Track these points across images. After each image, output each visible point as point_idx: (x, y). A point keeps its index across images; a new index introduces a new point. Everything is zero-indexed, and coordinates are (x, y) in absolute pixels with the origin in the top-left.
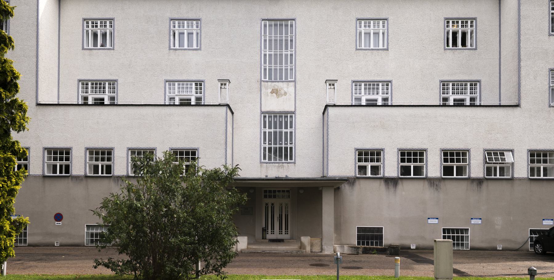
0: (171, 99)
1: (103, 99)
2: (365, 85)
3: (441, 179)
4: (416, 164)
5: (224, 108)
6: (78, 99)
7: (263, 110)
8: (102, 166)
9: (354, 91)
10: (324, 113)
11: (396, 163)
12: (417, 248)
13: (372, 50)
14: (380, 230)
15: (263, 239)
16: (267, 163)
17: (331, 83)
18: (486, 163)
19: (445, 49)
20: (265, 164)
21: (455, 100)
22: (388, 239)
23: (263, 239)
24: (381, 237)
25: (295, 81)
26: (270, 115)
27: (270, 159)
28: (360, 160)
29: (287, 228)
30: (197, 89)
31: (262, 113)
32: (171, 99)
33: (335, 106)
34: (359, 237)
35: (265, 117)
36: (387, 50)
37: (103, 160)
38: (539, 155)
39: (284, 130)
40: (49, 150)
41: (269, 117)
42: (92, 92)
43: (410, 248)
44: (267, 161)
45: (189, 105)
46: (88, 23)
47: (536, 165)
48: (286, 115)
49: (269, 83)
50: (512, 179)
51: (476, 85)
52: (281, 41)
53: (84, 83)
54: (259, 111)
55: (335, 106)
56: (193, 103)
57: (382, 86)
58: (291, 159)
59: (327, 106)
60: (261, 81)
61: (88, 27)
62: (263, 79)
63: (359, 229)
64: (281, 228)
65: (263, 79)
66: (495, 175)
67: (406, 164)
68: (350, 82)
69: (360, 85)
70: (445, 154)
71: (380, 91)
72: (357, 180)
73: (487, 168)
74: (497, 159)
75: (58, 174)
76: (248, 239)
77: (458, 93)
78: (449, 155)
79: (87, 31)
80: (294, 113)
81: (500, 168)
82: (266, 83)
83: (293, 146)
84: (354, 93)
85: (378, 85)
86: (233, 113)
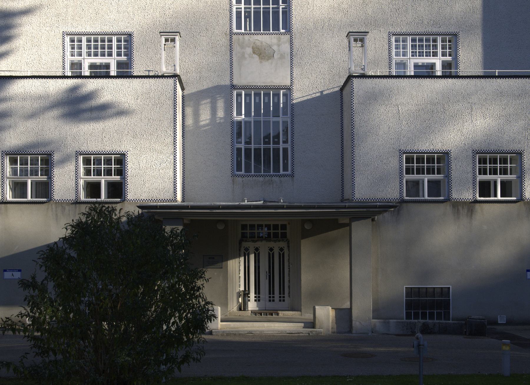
0: (73, 65)
1: (107, 66)
2: (413, 40)
4: (432, 177)
5: (171, 81)
6: (64, 68)
9: (394, 51)
12: (509, 322)
16: (242, 176)
17: (358, 37)
20: (240, 179)
21: (416, 66)
26: (248, 91)
27: (248, 169)
28: (483, 171)
29: (282, 291)
30: (73, 48)
32: (73, 65)
33: (363, 76)
39: (272, 119)
40: (123, 155)
42: (414, 54)
43: (496, 323)
44: (243, 172)
45: (107, 76)
48: (276, 92)
49: (247, 37)
53: (75, 38)
55: (363, 76)
56: (113, 73)
57: (396, 41)
58: (285, 169)
59: (350, 77)
60: (231, 33)
62: (235, 31)
64: (271, 291)
65: (235, 31)
66: (496, 196)
67: (415, 177)
69: (404, 41)
72: (404, 205)
77: (421, 54)
81: (502, 183)
82: (241, 37)
83: (288, 146)
84: (394, 53)
85: (435, 41)
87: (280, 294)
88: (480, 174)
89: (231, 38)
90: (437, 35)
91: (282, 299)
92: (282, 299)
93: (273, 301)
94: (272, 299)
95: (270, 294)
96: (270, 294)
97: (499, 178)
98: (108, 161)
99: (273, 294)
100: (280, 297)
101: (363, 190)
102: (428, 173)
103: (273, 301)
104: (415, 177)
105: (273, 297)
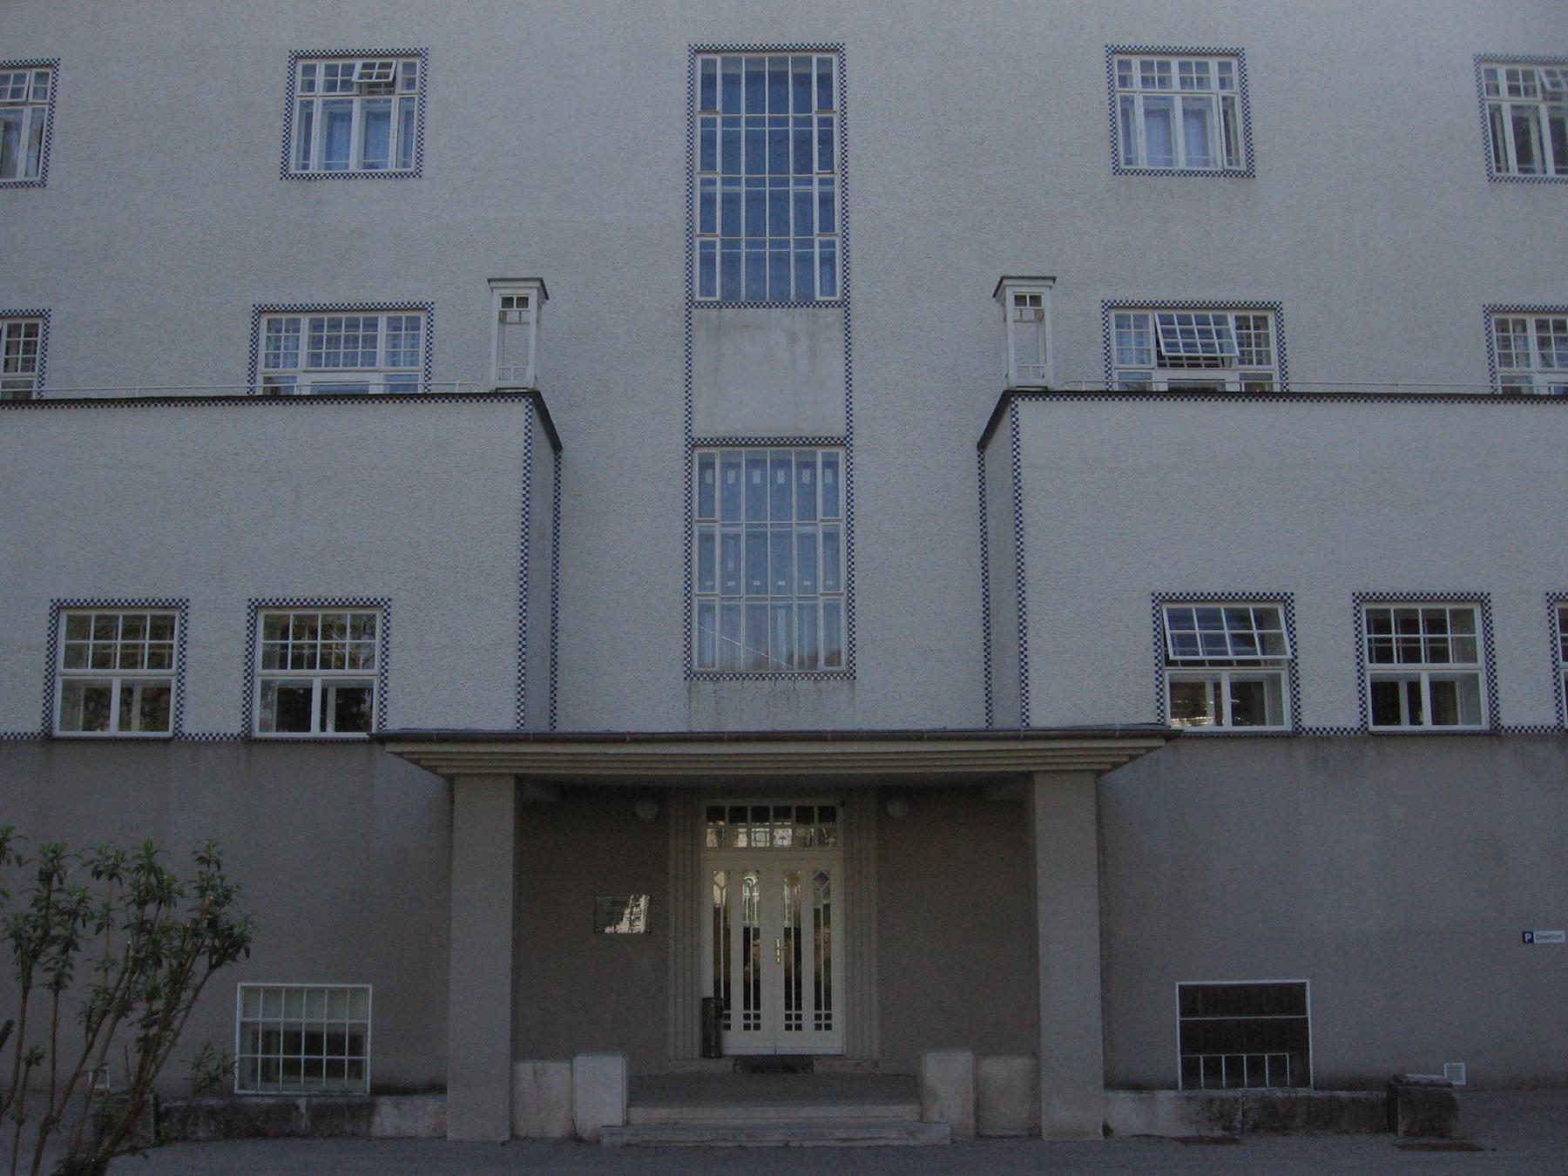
3: (1360, 737)
7: (699, 431)
8: (127, 691)
10: (982, 445)
11: (1350, 667)
13: (1183, 173)
14: (1292, 997)
15: (705, 1054)
18: (1169, 663)
19: (1491, 179)
22: (1337, 1042)
23: (705, 1054)
24: (1293, 1037)
25: (844, 304)
28: (1383, 655)
31: (693, 444)
34: (1192, 1039)
35: (707, 465)
36: (1249, 173)
37: (130, 661)
38: (105, 630)
41: (727, 466)
42: (315, 359)
46: (309, 70)
47: (1397, 669)
50: (1496, 733)
51: (1261, 322)
52: (779, 140)
54: (681, 438)
60: (691, 303)
61: (310, 86)
63: (1190, 998)
66: (1415, 720)
68: (1096, 311)
70: (1379, 623)
71: (382, 348)
73: (1376, 686)
74: (1215, 642)
75: (1427, 723)
76: (629, 1067)
78: (291, 631)
79: (307, 105)
80: (844, 442)
86: (557, 446)
87: (818, 1007)
88: (266, 665)
89: (688, 316)
90: (376, 310)
91: (793, 1022)
92: (793, 1022)
93: (799, 1027)
94: (823, 1022)
95: (788, 1007)
96: (788, 1006)
97: (1425, 671)
98: (133, 629)
99: (799, 1007)
100: (818, 1017)
101: (1056, 702)
102: (326, 664)
103: (799, 1027)
104: (290, 675)
105: (799, 1017)
